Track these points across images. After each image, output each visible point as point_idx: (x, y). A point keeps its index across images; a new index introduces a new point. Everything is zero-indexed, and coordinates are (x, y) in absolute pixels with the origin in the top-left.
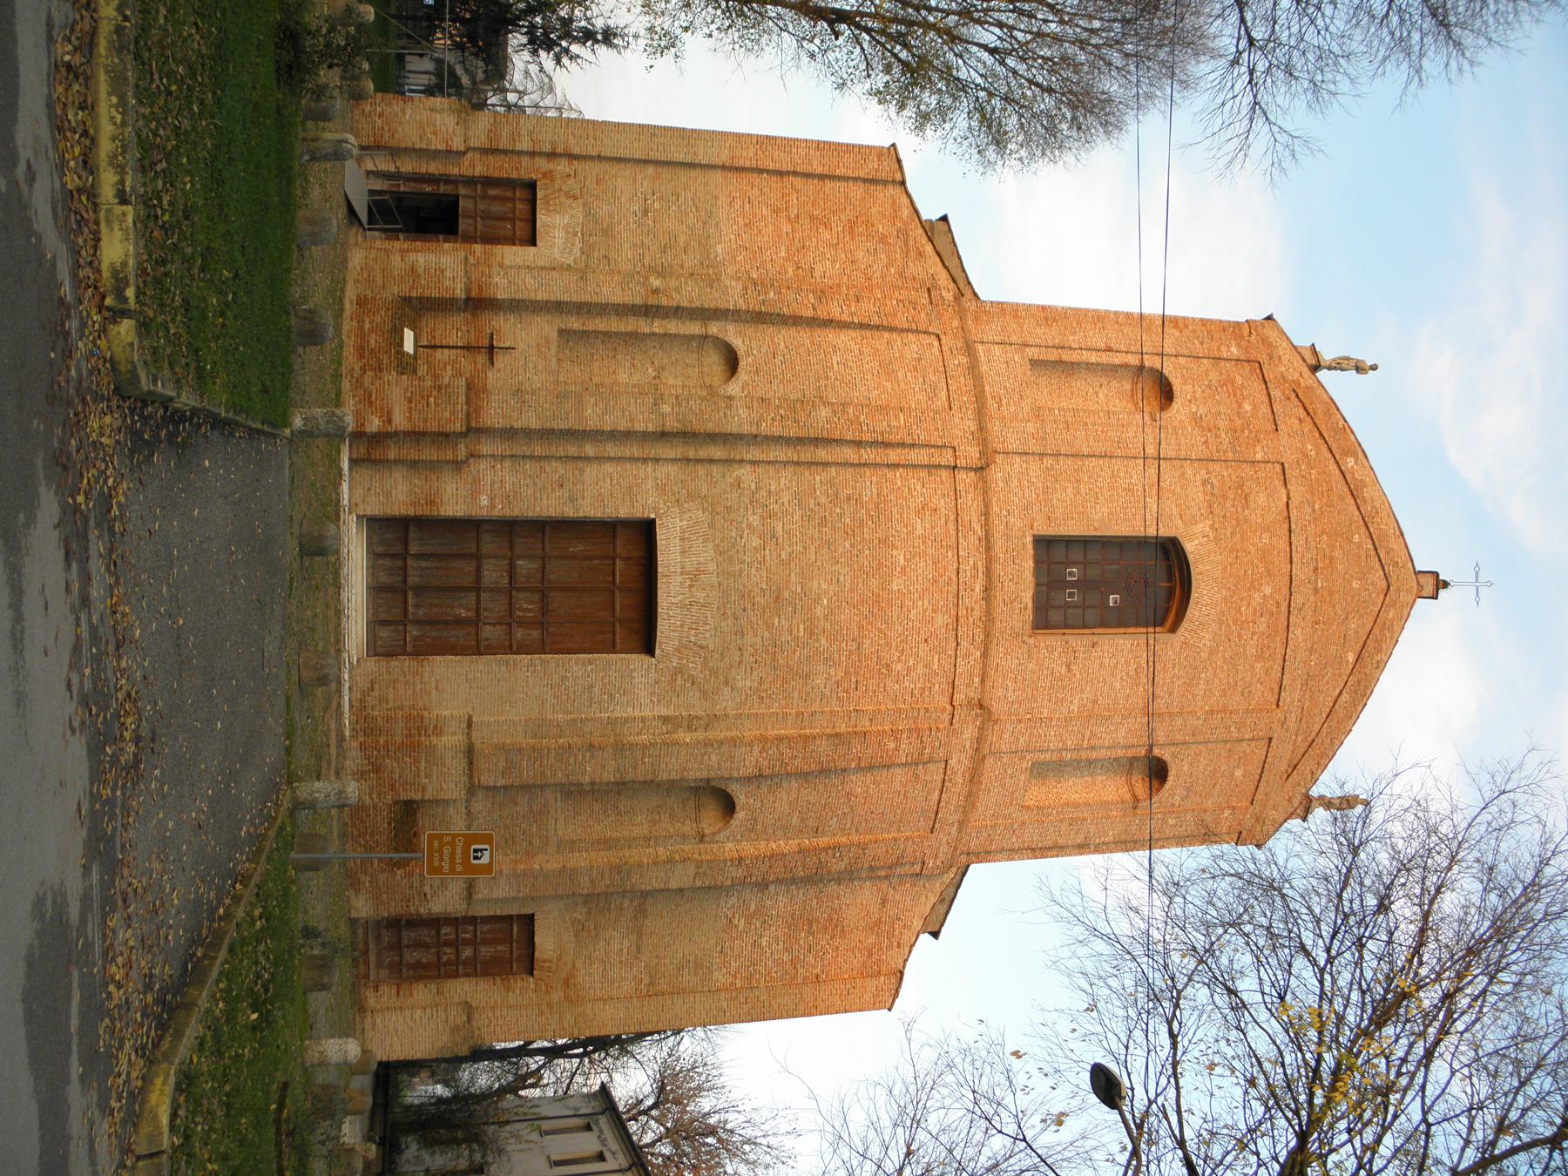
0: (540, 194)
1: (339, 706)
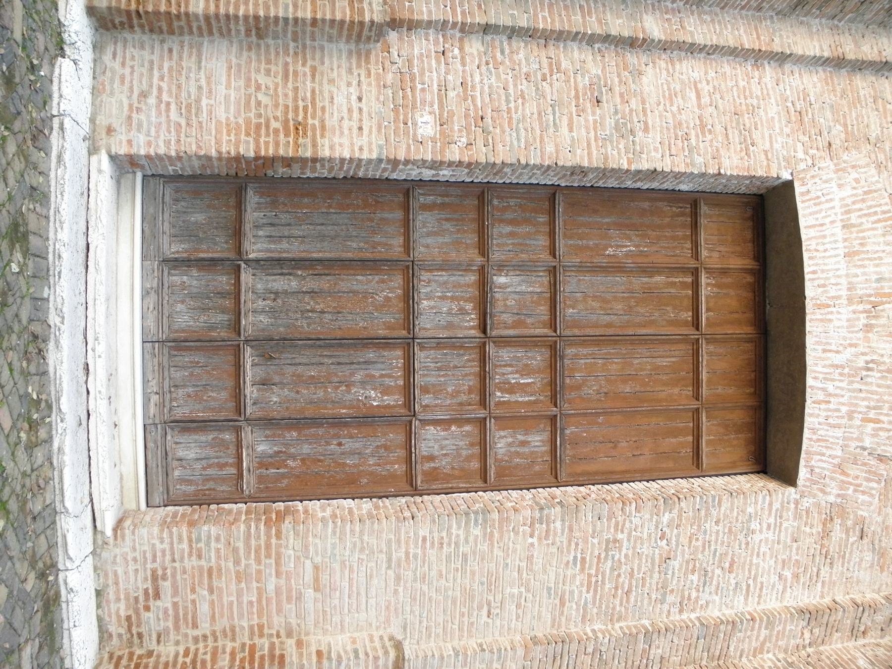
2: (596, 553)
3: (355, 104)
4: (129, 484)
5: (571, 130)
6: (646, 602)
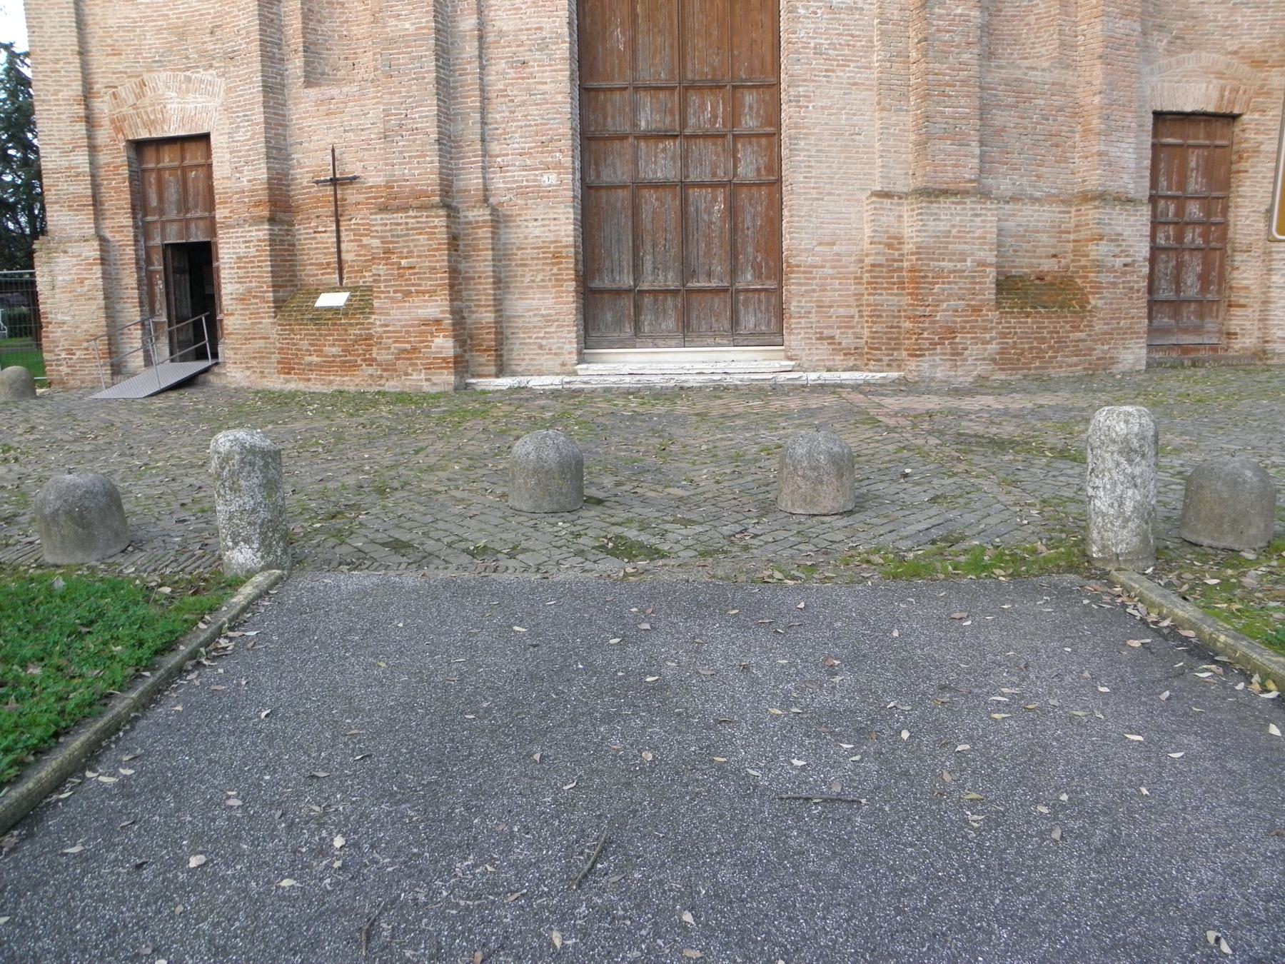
0: (144, 134)
1: (856, 388)
2: (822, 61)
3: (539, 223)
4: (769, 355)
5: (546, 83)
6: (860, 22)
